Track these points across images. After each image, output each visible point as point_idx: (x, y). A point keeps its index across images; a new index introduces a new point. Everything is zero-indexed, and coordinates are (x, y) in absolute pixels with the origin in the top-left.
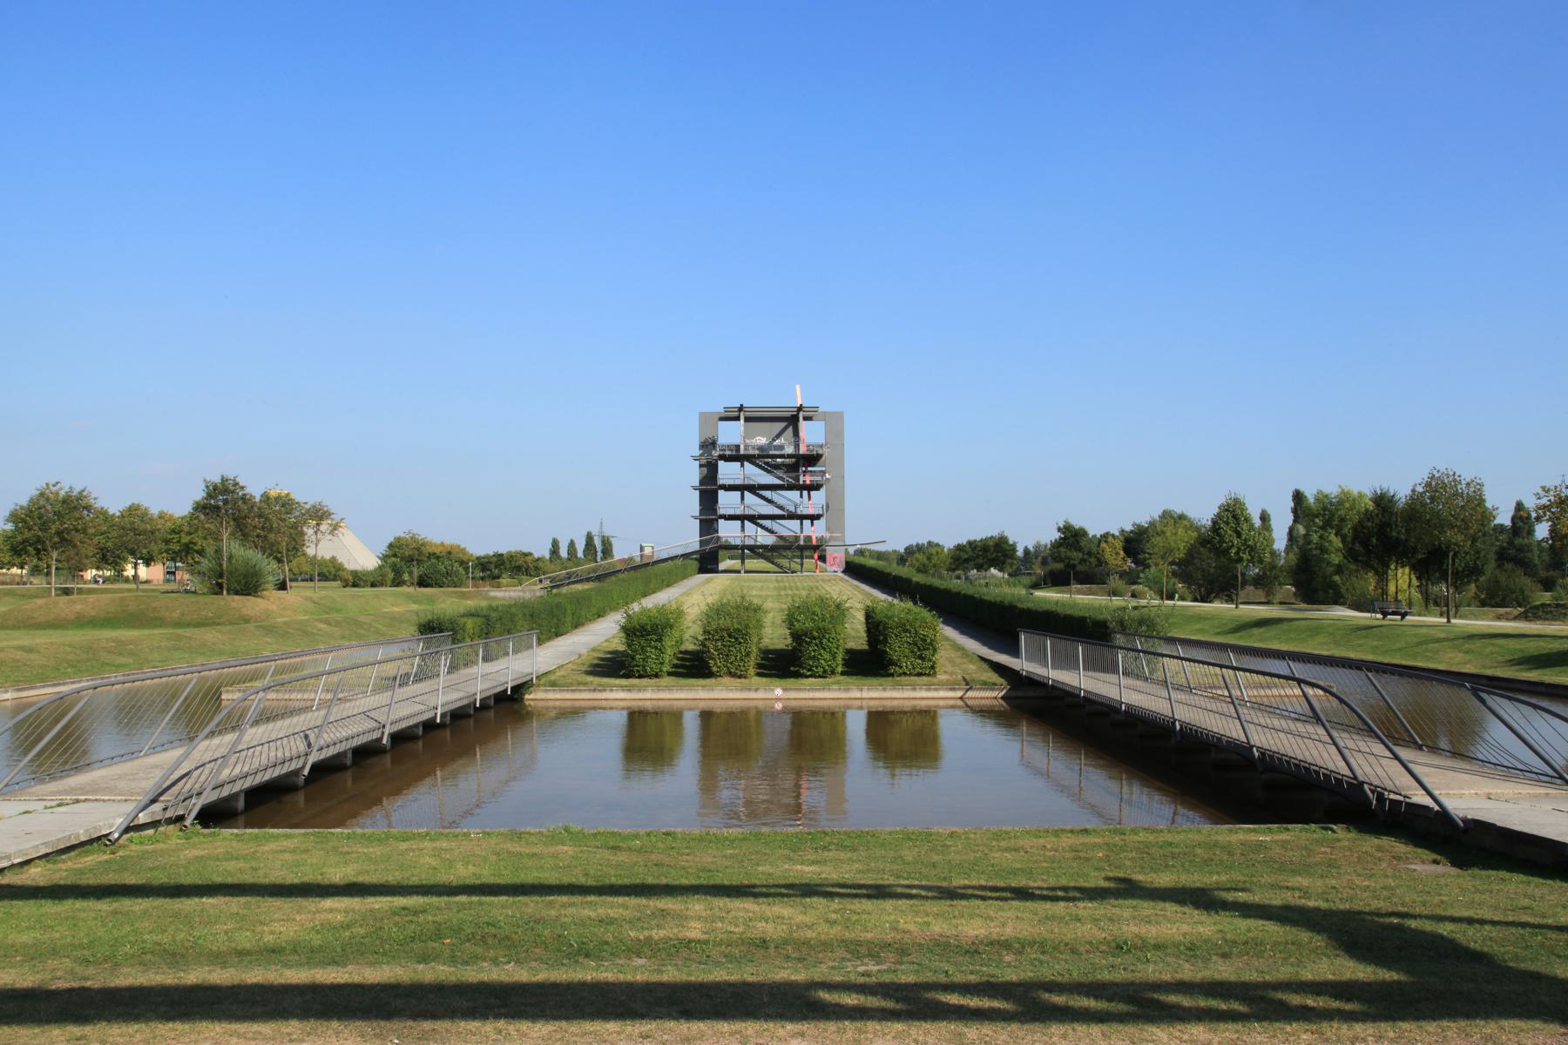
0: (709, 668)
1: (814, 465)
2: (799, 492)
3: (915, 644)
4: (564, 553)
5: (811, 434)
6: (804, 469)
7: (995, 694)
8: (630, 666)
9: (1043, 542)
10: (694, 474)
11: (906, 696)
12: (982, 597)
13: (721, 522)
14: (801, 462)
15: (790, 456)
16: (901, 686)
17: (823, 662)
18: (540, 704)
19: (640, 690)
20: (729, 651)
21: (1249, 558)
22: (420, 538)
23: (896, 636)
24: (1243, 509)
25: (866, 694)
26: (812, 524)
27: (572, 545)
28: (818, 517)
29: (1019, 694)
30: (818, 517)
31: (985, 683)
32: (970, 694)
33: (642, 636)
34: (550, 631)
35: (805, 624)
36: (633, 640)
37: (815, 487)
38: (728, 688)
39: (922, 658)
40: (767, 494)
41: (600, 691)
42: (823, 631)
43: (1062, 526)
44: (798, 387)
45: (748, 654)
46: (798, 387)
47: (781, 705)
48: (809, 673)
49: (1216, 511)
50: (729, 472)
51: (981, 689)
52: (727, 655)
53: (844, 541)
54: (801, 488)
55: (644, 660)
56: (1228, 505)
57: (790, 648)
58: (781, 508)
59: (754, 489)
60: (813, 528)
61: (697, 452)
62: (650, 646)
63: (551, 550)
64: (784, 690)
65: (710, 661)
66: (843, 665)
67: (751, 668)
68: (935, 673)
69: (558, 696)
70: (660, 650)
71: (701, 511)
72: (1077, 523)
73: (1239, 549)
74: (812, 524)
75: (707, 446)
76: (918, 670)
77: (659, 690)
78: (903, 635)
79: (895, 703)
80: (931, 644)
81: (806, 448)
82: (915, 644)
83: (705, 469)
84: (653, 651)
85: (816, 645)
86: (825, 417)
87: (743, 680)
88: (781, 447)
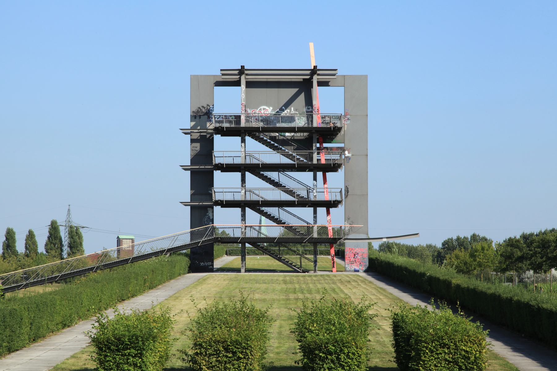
2: (311, 174)
6: (318, 145)
13: (217, 209)
14: (315, 137)
15: (301, 130)
26: (328, 213)
27: (31, 236)
28: (334, 204)
30: (334, 204)
33: (118, 350)
36: (106, 356)
37: (333, 167)
40: (273, 175)
42: (341, 345)
44: (311, 45)
46: (311, 45)
53: (367, 234)
54: (315, 168)
57: (300, 365)
58: (290, 192)
60: (329, 218)
61: (188, 124)
62: (128, 363)
63: (4, 243)
71: (192, 195)
74: (328, 213)
78: (440, 350)
81: (320, 121)
82: (456, 363)
83: (198, 145)
85: (332, 361)
86: (345, 81)
88: (291, 119)
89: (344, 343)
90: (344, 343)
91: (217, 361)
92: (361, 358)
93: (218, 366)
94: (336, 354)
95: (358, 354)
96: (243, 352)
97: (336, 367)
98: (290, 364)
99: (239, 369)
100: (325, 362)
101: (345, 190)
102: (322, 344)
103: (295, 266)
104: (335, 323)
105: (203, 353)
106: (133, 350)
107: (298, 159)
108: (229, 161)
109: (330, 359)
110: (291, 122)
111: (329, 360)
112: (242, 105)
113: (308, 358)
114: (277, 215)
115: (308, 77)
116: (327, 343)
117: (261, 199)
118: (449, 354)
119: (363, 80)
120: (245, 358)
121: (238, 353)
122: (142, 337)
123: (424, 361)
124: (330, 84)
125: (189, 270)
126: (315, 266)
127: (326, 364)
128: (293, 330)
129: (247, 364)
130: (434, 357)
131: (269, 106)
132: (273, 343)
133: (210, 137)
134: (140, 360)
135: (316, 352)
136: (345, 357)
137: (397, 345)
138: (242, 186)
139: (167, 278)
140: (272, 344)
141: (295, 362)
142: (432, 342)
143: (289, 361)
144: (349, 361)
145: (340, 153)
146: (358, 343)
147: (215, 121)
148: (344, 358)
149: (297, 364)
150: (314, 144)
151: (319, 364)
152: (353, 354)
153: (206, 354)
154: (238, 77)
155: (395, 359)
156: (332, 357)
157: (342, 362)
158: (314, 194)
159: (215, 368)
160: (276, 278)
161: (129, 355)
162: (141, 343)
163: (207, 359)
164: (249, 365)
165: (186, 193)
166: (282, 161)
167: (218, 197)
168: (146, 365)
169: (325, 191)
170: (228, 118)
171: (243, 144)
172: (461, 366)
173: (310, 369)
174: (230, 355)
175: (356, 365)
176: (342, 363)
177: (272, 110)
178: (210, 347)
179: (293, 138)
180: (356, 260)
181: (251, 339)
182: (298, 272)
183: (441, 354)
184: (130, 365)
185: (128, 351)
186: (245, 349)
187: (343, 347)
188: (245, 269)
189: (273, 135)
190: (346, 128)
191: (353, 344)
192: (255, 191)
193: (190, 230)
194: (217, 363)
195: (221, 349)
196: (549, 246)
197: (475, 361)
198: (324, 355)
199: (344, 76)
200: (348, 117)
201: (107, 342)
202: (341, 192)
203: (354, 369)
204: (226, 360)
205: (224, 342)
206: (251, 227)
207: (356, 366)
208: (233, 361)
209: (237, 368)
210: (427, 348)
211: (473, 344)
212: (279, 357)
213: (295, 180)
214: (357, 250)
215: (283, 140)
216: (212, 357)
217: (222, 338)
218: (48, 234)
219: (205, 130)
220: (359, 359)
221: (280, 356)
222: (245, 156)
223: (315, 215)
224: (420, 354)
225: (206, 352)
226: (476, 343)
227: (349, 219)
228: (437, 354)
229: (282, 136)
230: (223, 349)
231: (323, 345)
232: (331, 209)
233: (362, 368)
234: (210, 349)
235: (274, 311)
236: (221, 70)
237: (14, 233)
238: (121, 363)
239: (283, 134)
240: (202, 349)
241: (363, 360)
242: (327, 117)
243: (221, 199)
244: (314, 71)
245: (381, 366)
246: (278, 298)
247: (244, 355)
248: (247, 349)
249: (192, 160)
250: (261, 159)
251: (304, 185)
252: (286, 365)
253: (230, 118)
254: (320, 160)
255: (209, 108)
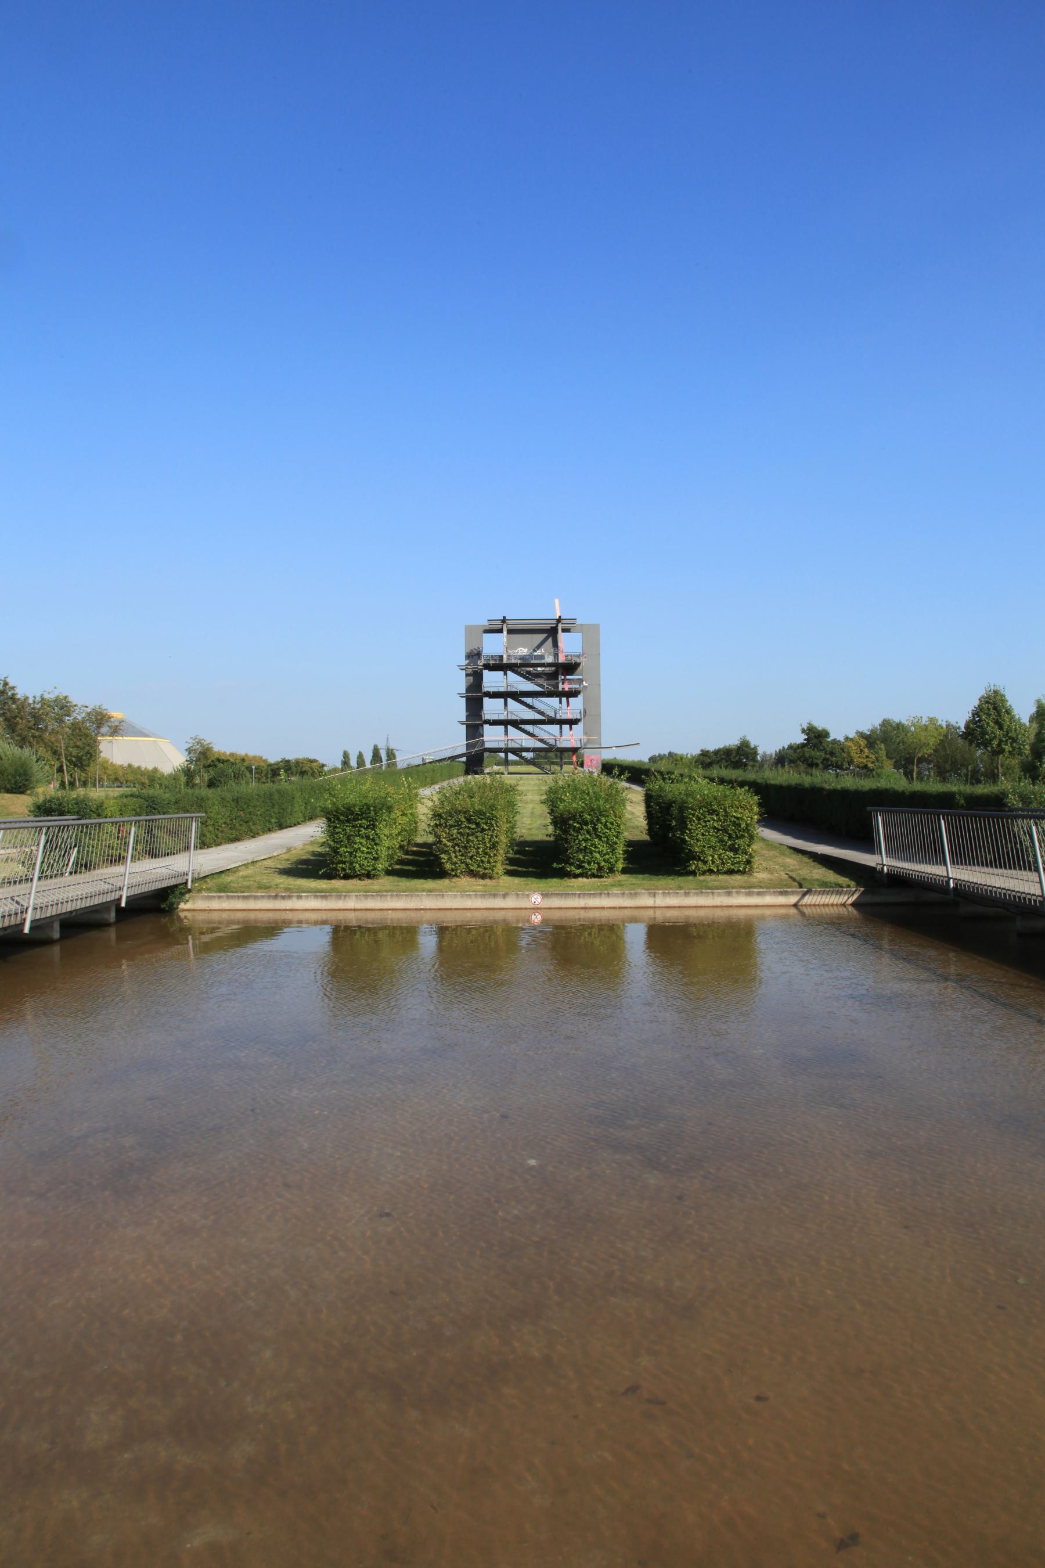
0: (441, 865)
1: (572, 674)
3: (725, 831)
4: (353, 763)
5: (569, 645)
7: (842, 899)
8: (333, 863)
9: (768, 753)
10: (460, 683)
11: (719, 904)
12: (768, 782)
13: (486, 727)
14: (561, 671)
15: (549, 665)
16: (712, 888)
17: (597, 855)
18: (200, 917)
19: (339, 897)
20: (468, 841)
21: (1011, 749)
22: (205, 743)
23: (699, 819)
24: (1003, 700)
25: (660, 901)
26: (571, 729)
27: (360, 756)
28: (576, 722)
29: (877, 899)
30: (576, 722)
31: (824, 884)
32: (808, 899)
33: (348, 821)
34: (270, 822)
35: (570, 804)
36: (336, 827)
37: (574, 694)
38: (464, 893)
39: (734, 849)
40: (529, 700)
41: (283, 898)
42: (598, 814)
43: (806, 728)
44: (557, 601)
45: (494, 846)
46: (557, 601)
47: (539, 917)
48: (578, 871)
49: (977, 703)
50: (493, 680)
51: (823, 893)
52: (465, 847)
53: (600, 745)
54: (561, 694)
55: (351, 853)
56: (988, 697)
59: (516, 696)
60: (571, 732)
61: (464, 662)
62: (359, 835)
63: (342, 761)
64: (545, 895)
65: (443, 856)
66: (624, 860)
67: (499, 865)
68: (751, 870)
69: (226, 905)
70: (373, 840)
72: (820, 725)
73: (1001, 741)
74: (571, 729)
75: (472, 656)
76: (729, 866)
77: (366, 897)
78: (708, 817)
79: (702, 913)
80: (747, 830)
81: (564, 658)
82: (725, 831)
83: (471, 679)
84: (364, 841)
85: (588, 832)
86: (582, 628)
87: (487, 881)
88: (542, 657)
90: (601, 812)
91: (458, 833)
95: (617, 823)
104: (589, 792)
106: (364, 821)
107: (547, 688)
108: (495, 690)
115: (555, 625)
116: (582, 812)
118: (717, 821)
119: (596, 628)
120: (489, 829)
122: (374, 807)
123: (690, 830)
127: (581, 835)
129: (492, 836)
130: (701, 825)
131: (525, 648)
134: (373, 832)
136: (603, 827)
137: (650, 816)
138: (505, 709)
140: (524, 821)
142: (700, 809)
146: (617, 812)
148: (601, 828)
150: (559, 676)
151: (573, 835)
152: (612, 823)
153: (446, 826)
157: (600, 832)
161: (361, 826)
162: (372, 813)
163: (448, 831)
164: (494, 837)
165: (462, 715)
167: (486, 717)
168: (379, 838)
171: (505, 677)
172: (731, 834)
174: (473, 826)
175: (614, 836)
182: (549, 774)
183: (709, 821)
184: (362, 837)
185: (360, 822)
186: (490, 819)
187: (600, 815)
193: (465, 742)
194: (459, 836)
195: (463, 819)
196: (731, 754)
197: (746, 828)
200: (586, 655)
201: (336, 812)
202: (580, 712)
210: (693, 815)
211: (745, 810)
212: (531, 833)
213: (545, 731)
214: (593, 757)
216: (453, 828)
218: (372, 754)
224: (686, 822)
225: (446, 824)
226: (747, 809)
228: (705, 821)
229: (534, 670)
232: (573, 726)
236: (488, 620)
237: (349, 754)
238: (352, 835)
239: (536, 668)
240: (442, 820)
244: (559, 620)
248: (492, 819)
249: (466, 690)
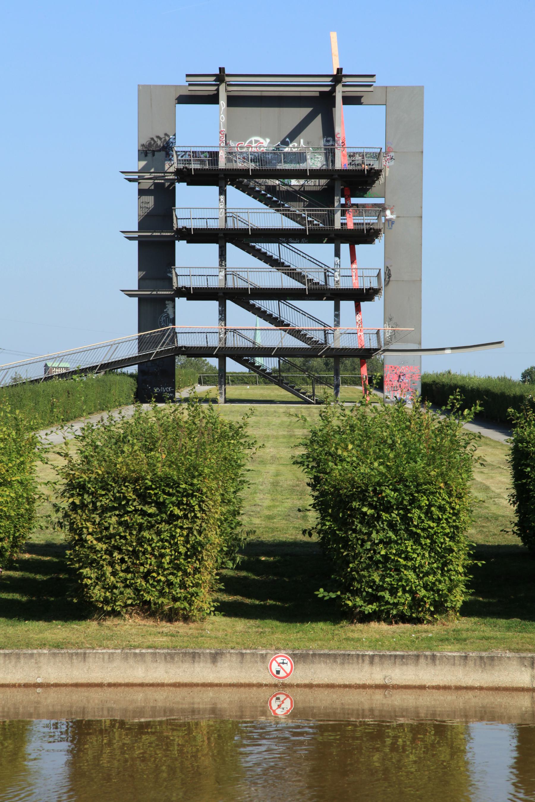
1: (362, 195)
2: (332, 246)
6: (343, 201)
13: (181, 302)
14: (339, 187)
15: (315, 174)
17: (411, 575)
20: (140, 541)
26: (358, 309)
44: (334, 36)
46: (334, 36)
47: (287, 705)
48: (369, 608)
52: (135, 554)
53: (420, 344)
57: (315, 538)
58: (296, 333)
60: (359, 317)
65: (86, 571)
67: (204, 592)
71: (140, 280)
74: (358, 309)
75: (153, 152)
81: (347, 161)
83: (150, 200)
85: (392, 526)
87: (179, 626)
88: (301, 157)
89: (419, 485)
90: (419, 485)
91: (120, 523)
92: (458, 518)
93: (123, 534)
94: (401, 509)
95: (453, 509)
96: (183, 504)
97: (401, 539)
98: (293, 537)
99: (172, 542)
100: (376, 526)
101: (385, 273)
102: (367, 485)
103: (304, 393)
105: (87, 506)
108: (201, 225)
109: (386, 521)
110: (299, 163)
111: (383, 523)
112: (220, 133)
113: (335, 518)
114: (277, 311)
115: (327, 89)
116: (379, 484)
117: (250, 287)
120: (186, 516)
121: (170, 505)
124: (363, 100)
125: (135, 398)
126: (337, 394)
128: (299, 460)
129: (190, 529)
131: (264, 137)
132: (261, 499)
133: (169, 186)
135: (354, 504)
136: (423, 516)
138: (221, 265)
139: (95, 406)
140: (258, 502)
141: (304, 532)
143: (292, 531)
144: (432, 525)
145: (377, 214)
147: (177, 160)
148: (420, 518)
149: (307, 535)
150: (336, 198)
151: (361, 532)
152: (442, 509)
153: (95, 508)
154: (215, 88)
155: (516, 528)
156: (391, 516)
157: (416, 527)
158: (336, 279)
159: (115, 541)
160: (273, 410)
163: (98, 520)
164: (195, 533)
166: (284, 225)
169: (354, 274)
170: (198, 156)
171: (222, 197)
173: (338, 544)
174: (152, 510)
175: (447, 535)
176: (414, 529)
177: (269, 143)
178: (104, 490)
179: (302, 189)
180: (402, 384)
181: (200, 475)
186: (187, 496)
187: (418, 492)
188: (225, 398)
189: (270, 184)
190: (386, 173)
191: (442, 485)
192: (241, 274)
194: (121, 529)
195: (131, 495)
198: (373, 511)
199: (386, 87)
200: (392, 154)
202: (379, 275)
203: (442, 543)
204: (141, 521)
205: (136, 480)
206: (234, 331)
207: (448, 537)
208: (159, 523)
209: (166, 541)
212: (271, 525)
214: (403, 369)
215: (287, 191)
216: (109, 514)
217: (134, 471)
219: (160, 175)
220: (454, 521)
221: (273, 523)
222: (226, 217)
223: (337, 313)
225: (94, 503)
227: (390, 319)
230: (134, 497)
231: (371, 489)
233: (461, 542)
234: (103, 495)
235: (268, 451)
236: (188, 76)
239: (286, 181)
240: (86, 496)
241: (464, 522)
242: (357, 156)
243: (187, 285)
245: (483, 543)
246: (275, 434)
247: (185, 510)
248: (192, 496)
249: (139, 224)
250: (250, 221)
251: (318, 263)
252: (284, 540)
253: (202, 156)
254: (345, 224)
255: (167, 138)
